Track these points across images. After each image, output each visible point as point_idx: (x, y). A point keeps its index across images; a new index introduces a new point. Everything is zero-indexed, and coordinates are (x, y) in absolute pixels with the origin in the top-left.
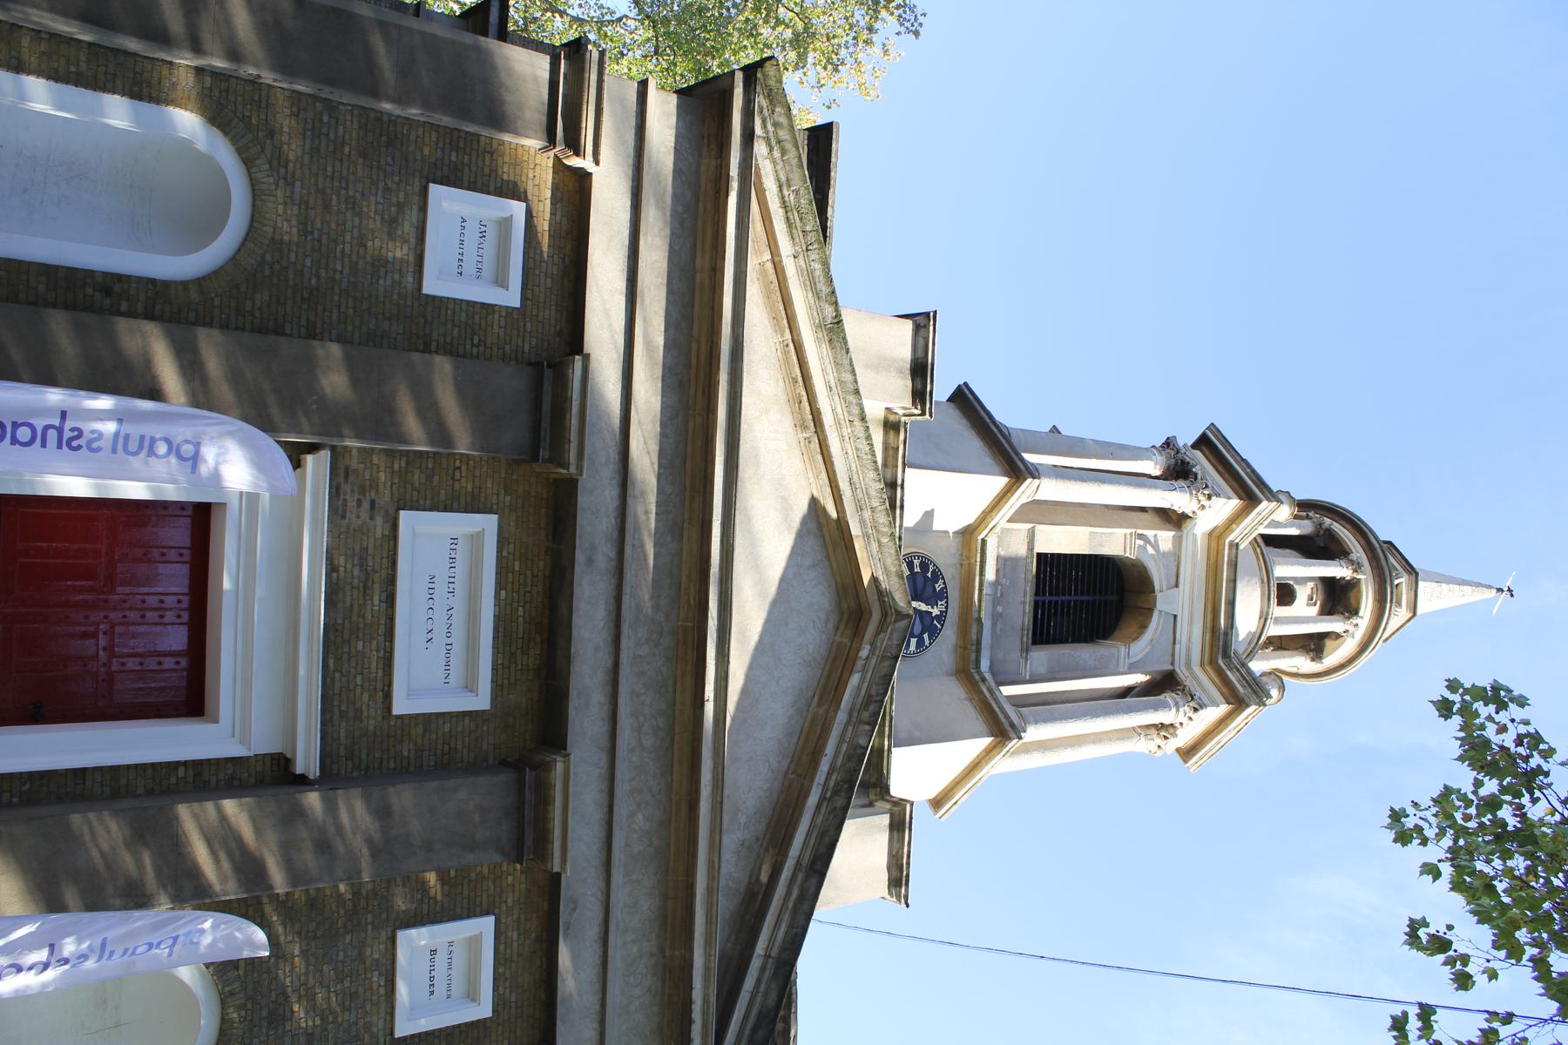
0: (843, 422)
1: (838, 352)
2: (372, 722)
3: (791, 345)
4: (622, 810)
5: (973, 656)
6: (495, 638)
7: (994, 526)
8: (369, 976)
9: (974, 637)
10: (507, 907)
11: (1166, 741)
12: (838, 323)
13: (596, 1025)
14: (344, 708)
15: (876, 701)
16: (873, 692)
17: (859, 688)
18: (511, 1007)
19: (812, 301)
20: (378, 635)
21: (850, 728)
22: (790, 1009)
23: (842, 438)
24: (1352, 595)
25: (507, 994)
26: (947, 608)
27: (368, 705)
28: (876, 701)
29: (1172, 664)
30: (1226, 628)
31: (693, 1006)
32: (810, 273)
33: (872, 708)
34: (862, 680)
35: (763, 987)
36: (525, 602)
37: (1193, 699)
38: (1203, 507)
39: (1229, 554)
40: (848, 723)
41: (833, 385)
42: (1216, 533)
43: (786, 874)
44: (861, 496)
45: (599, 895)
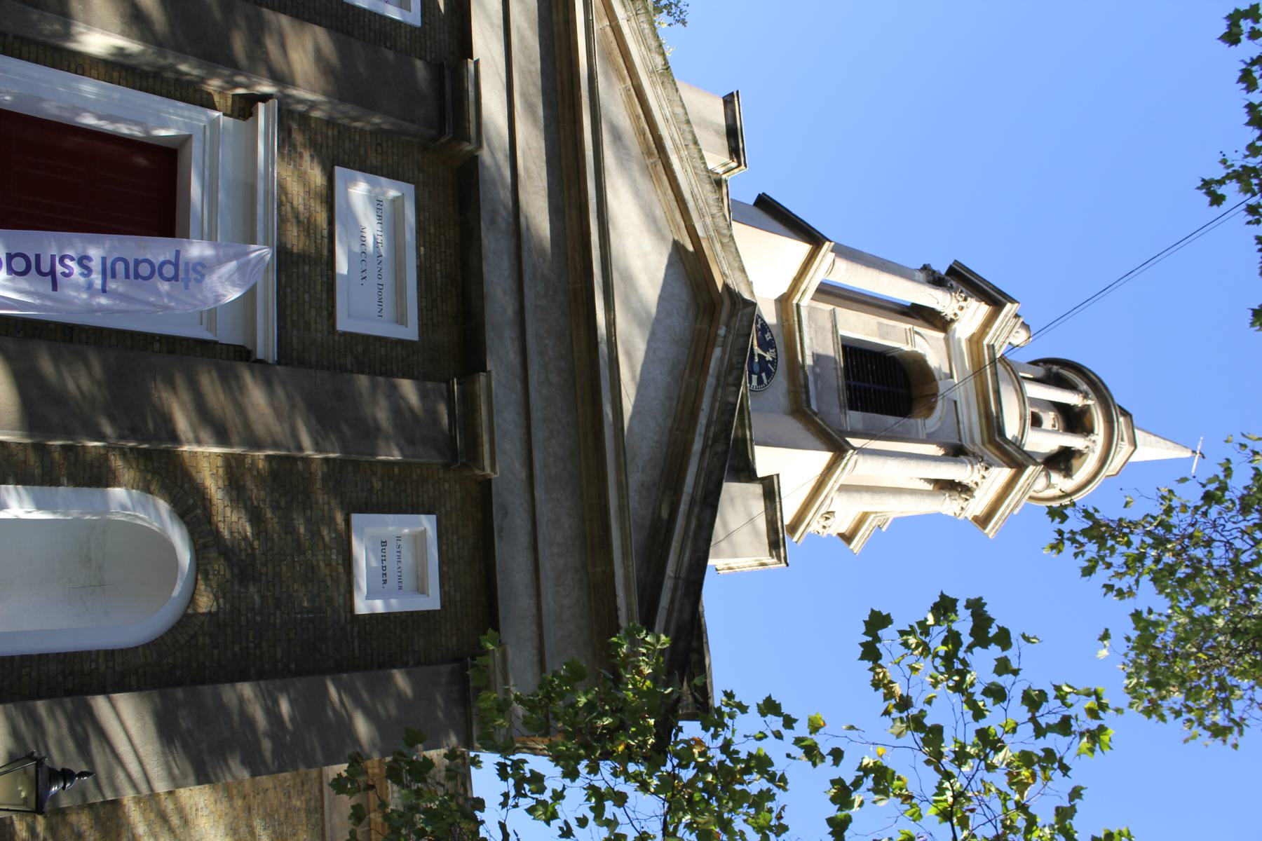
0: (680, 146)
1: (670, 90)
2: (319, 335)
3: (632, 90)
4: (539, 434)
5: (804, 397)
6: (419, 284)
7: (805, 290)
8: (328, 552)
9: (802, 382)
10: (446, 511)
11: (967, 502)
12: (667, 69)
13: (534, 628)
14: (295, 318)
15: (738, 368)
16: (734, 361)
17: (722, 359)
18: (456, 605)
19: (645, 53)
20: (322, 263)
21: (720, 390)
22: (702, 639)
23: (681, 159)
24: (1086, 420)
25: (452, 593)
26: (777, 355)
27: (316, 321)
28: (738, 368)
29: (960, 440)
30: (997, 412)
31: (619, 613)
32: (642, 32)
33: (735, 373)
34: (724, 352)
35: (677, 604)
36: (441, 261)
37: (982, 460)
38: (961, 308)
39: (989, 353)
40: (717, 386)
41: (669, 117)
42: (975, 339)
43: (683, 508)
44: (702, 205)
45: (525, 505)
